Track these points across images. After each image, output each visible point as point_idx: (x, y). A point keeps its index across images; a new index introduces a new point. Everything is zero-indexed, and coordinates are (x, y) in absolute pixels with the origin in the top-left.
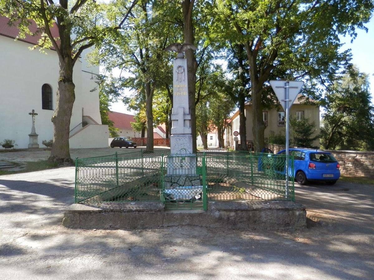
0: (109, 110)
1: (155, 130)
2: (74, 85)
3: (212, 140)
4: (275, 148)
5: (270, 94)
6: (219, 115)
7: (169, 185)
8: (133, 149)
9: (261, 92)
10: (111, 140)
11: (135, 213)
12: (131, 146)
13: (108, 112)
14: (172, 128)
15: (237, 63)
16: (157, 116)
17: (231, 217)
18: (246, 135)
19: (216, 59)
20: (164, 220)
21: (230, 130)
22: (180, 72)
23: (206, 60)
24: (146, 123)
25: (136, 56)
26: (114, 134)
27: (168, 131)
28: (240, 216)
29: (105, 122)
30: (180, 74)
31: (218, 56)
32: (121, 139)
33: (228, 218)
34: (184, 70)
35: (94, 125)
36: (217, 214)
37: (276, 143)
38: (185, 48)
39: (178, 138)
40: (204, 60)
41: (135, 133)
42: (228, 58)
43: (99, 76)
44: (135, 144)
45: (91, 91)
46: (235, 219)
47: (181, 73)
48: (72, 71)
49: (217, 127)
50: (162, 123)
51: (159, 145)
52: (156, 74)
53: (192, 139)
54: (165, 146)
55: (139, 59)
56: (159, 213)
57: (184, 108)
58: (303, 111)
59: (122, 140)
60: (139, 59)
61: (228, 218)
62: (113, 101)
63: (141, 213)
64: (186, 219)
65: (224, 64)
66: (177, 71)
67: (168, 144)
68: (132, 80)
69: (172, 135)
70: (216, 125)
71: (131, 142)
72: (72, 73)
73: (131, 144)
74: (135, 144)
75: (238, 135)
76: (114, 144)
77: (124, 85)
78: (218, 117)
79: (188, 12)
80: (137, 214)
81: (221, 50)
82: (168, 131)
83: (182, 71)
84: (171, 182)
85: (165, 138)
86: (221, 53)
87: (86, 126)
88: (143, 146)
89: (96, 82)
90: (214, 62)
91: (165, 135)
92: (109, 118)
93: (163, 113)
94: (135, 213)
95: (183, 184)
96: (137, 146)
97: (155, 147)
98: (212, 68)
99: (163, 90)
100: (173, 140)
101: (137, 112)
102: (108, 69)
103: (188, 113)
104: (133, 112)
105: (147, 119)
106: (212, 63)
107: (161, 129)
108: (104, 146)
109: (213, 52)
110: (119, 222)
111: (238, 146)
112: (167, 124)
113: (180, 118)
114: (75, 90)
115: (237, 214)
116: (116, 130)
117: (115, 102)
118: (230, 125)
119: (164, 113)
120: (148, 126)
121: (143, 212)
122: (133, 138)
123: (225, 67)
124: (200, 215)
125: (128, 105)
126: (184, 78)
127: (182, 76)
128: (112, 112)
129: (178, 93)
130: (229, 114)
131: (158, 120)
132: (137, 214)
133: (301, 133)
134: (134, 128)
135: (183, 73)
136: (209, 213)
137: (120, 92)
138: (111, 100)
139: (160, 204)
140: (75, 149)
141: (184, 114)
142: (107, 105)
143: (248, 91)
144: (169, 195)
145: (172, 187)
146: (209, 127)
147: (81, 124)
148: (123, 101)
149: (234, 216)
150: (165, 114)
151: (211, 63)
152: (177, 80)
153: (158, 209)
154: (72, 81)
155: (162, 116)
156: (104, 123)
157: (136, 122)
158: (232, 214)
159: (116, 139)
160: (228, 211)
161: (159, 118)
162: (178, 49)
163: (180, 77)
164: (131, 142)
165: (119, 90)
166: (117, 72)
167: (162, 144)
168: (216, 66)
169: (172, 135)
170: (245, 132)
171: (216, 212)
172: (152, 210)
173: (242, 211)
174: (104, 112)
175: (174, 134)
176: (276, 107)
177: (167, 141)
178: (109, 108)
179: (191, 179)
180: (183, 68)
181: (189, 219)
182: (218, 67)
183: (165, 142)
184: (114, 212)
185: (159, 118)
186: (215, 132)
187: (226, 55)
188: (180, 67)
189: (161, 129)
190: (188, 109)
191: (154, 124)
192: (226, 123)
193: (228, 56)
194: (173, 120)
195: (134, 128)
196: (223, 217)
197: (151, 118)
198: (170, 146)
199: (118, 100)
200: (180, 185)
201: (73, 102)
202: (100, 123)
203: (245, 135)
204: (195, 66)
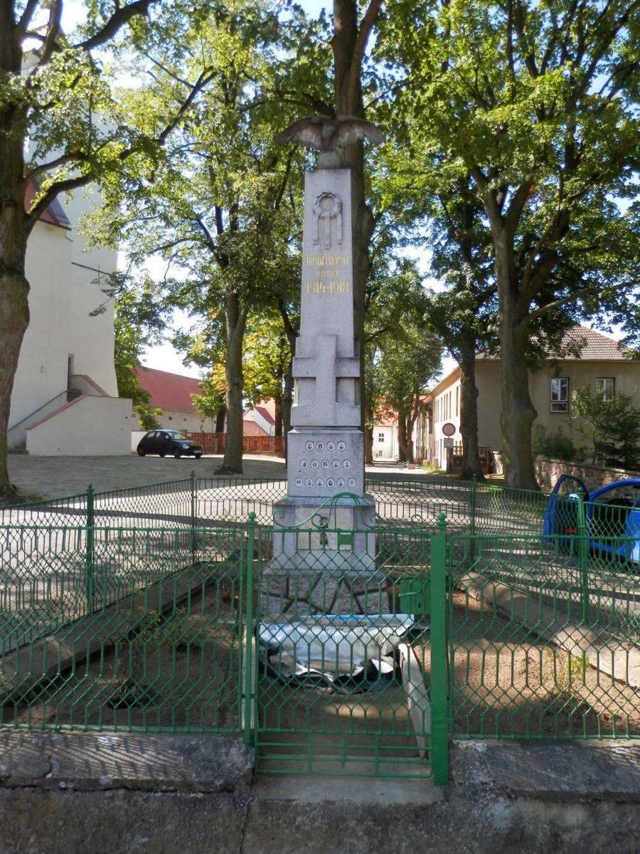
0: (138, 363)
1: (250, 416)
2: (26, 286)
3: (381, 443)
4: (554, 470)
5: (538, 335)
6: (402, 383)
7: (276, 606)
8: (193, 461)
9: (524, 323)
10: (137, 437)
11: (112, 798)
12: (189, 452)
13: (137, 368)
14: (295, 405)
15: (456, 255)
16: (255, 380)
17: (568, 830)
18: (478, 434)
19: (404, 245)
20: (248, 836)
21: (428, 420)
22: (326, 214)
23: (379, 247)
24: (226, 397)
25: (206, 227)
26: (149, 423)
27: (283, 418)
28: (610, 828)
29: (126, 391)
30: (327, 220)
31: (409, 237)
32: (164, 434)
33: (555, 836)
34: (341, 206)
35: (97, 399)
36: (501, 812)
37: (556, 457)
38: (347, 135)
39: (315, 439)
40: (374, 246)
41: (203, 421)
42: (435, 243)
43: (113, 276)
44: (199, 448)
45: (91, 315)
46: (587, 839)
47: (331, 218)
48: (23, 247)
49: (397, 414)
50: (268, 400)
51: (259, 454)
52: (253, 273)
53: (362, 448)
54: (272, 454)
55: (214, 234)
56: (224, 804)
57: (337, 338)
58: (614, 379)
59: (167, 437)
60: (214, 234)
61: (555, 838)
62: (149, 342)
63: (139, 797)
64: (354, 833)
65: (423, 257)
66: (318, 211)
67: (282, 451)
68: (192, 287)
69: (294, 431)
70: (396, 407)
71: (188, 444)
72: (23, 252)
73: (187, 447)
74: (199, 448)
75: (453, 433)
76: (146, 447)
77: (172, 301)
78: (401, 389)
79: (349, 64)
80: (118, 803)
81: (417, 221)
82: (283, 418)
83: (336, 209)
84: (286, 596)
85: (274, 435)
86: (415, 231)
87: (77, 399)
88: (218, 453)
89: (104, 291)
90: (399, 253)
91: (273, 428)
92: (139, 383)
93: (269, 375)
94: (112, 798)
95: (328, 606)
96: (202, 454)
97: (245, 457)
98: (392, 265)
99: (271, 315)
100: (293, 445)
101: (206, 370)
102: (136, 258)
103: (352, 355)
104: (195, 372)
105: (228, 389)
106: (393, 254)
107: (263, 412)
108: (121, 452)
109: (395, 228)
110: (32, 840)
111: (453, 461)
112: (278, 402)
113: (324, 371)
114: (30, 298)
115: (595, 816)
116: (155, 413)
117: (156, 344)
118: (428, 409)
119: (273, 374)
120: (230, 405)
121: (150, 790)
122: (195, 435)
123: (424, 266)
124: (419, 814)
125: (184, 354)
126: (339, 236)
127: (333, 228)
128: (145, 369)
129: (318, 287)
130: (425, 382)
131: (258, 392)
132: (118, 803)
133: (614, 431)
134: (199, 409)
135: (339, 218)
136: (460, 807)
137: (162, 316)
138: (145, 340)
139: (234, 751)
140: (44, 457)
141: (339, 359)
142: (136, 351)
143: (485, 321)
144: (273, 650)
145: (289, 616)
146: (377, 413)
147: (65, 396)
148: (174, 342)
149: (582, 827)
150: (276, 378)
151: (390, 255)
152: (317, 242)
153: (218, 783)
154: (21, 273)
155: (267, 381)
156: (123, 394)
157: (204, 393)
158: (574, 816)
159: (152, 435)
160: (555, 801)
161: (260, 387)
162: (323, 139)
163: (327, 230)
164: (188, 444)
165: (161, 314)
166: (157, 268)
167: (266, 449)
168: (402, 262)
169: (292, 428)
170: (475, 425)
171: (495, 801)
172: (189, 787)
173: (620, 803)
174: (128, 369)
175: (299, 427)
176: (552, 366)
177: (279, 444)
178: (140, 358)
179: (357, 589)
180: (336, 200)
181: (369, 833)
182: (407, 265)
183: (272, 444)
184: (14, 788)
185: (260, 387)
186: (390, 424)
187: (429, 234)
188: (326, 196)
189: (263, 412)
190: (352, 341)
191: (245, 402)
192: (419, 402)
193: (435, 237)
194: (298, 379)
195: (199, 409)
196: (530, 829)
197: (237, 384)
198: (285, 456)
199: (162, 340)
200: (318, 610)
201: (23, 331)
202: (114, 391)
203: (475, 434)
204: (365, 225)
